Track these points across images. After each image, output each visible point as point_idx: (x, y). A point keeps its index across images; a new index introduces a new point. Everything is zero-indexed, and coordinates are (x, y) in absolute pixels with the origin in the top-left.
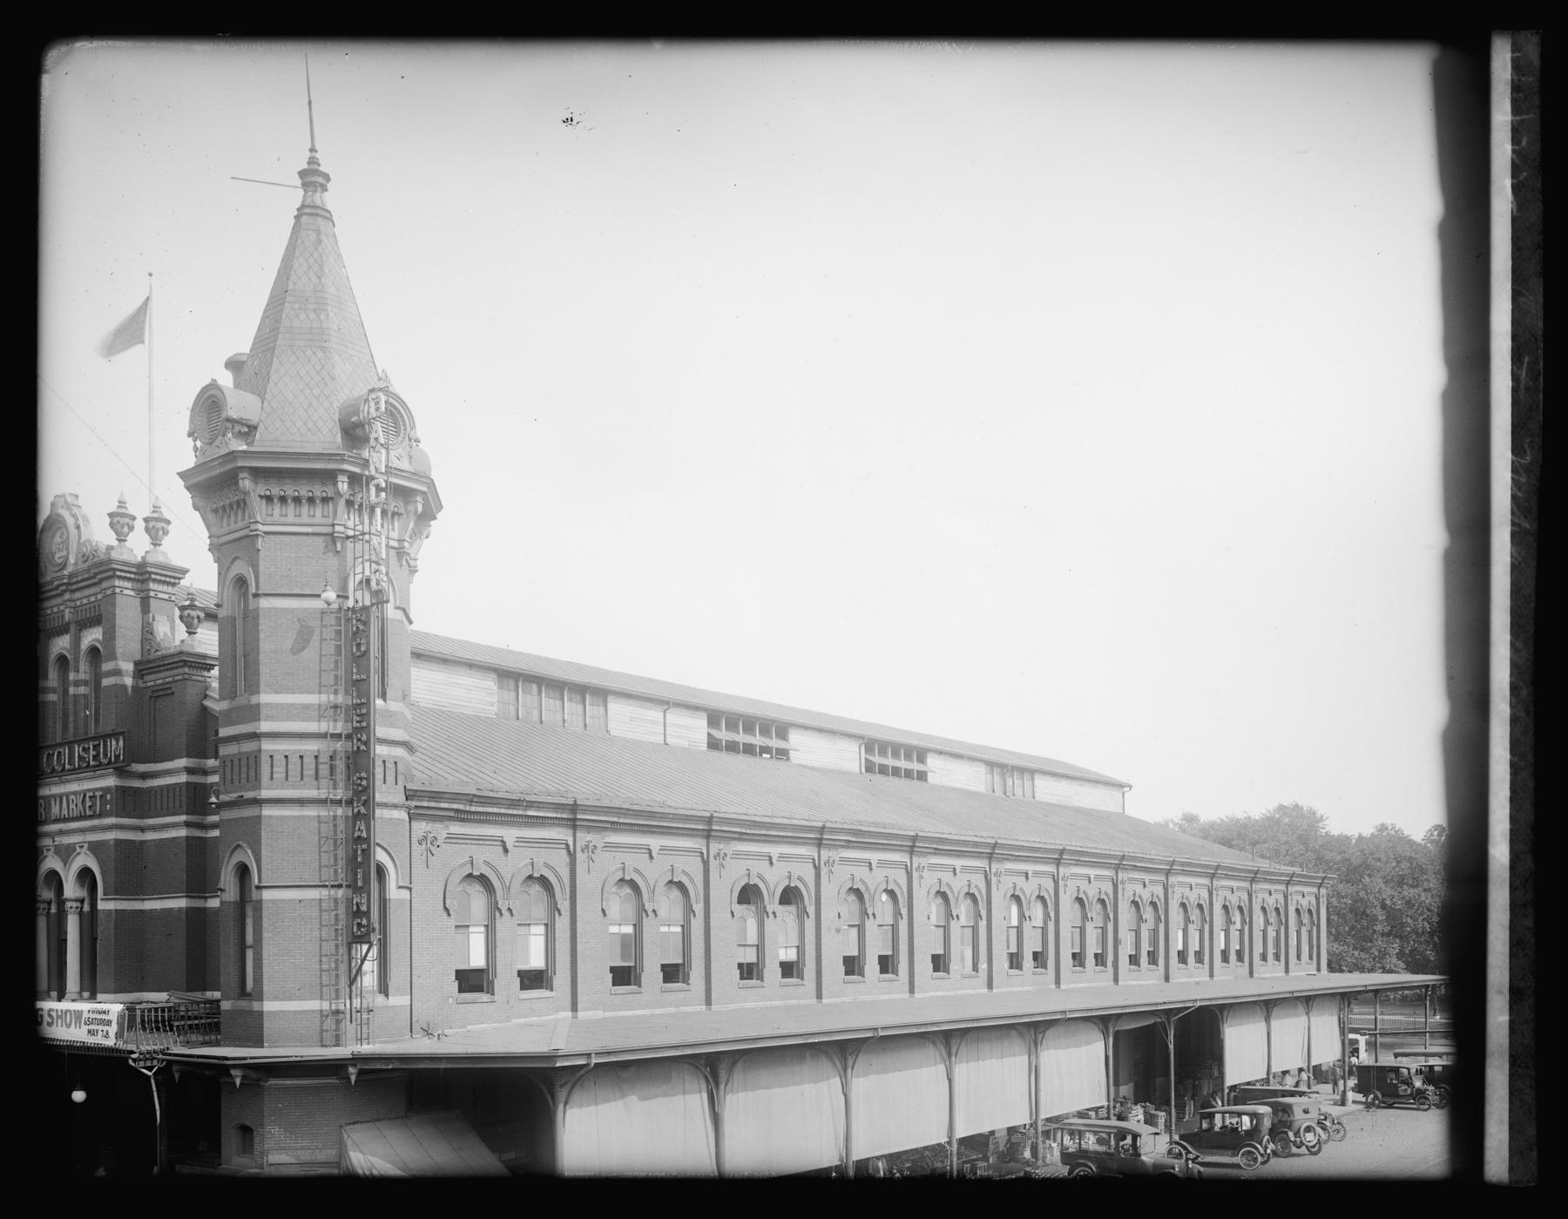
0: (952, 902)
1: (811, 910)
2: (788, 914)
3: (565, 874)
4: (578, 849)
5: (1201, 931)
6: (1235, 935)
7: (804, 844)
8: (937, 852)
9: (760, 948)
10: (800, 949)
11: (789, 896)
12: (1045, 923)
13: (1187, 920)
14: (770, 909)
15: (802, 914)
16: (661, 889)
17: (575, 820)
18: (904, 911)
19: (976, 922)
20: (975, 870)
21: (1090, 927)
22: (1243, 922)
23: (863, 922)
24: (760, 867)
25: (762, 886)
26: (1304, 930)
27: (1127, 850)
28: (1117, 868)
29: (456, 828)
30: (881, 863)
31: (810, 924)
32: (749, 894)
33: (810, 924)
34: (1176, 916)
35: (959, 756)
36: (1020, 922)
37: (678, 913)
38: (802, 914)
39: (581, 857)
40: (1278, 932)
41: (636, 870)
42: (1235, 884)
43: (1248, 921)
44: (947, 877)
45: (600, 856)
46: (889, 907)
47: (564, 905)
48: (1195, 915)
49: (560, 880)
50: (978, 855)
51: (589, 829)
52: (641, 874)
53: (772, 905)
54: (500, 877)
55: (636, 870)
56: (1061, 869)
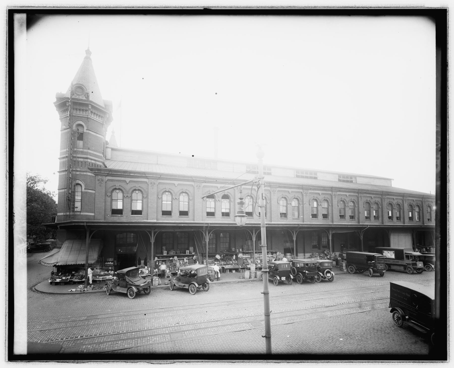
25: (229, 194)
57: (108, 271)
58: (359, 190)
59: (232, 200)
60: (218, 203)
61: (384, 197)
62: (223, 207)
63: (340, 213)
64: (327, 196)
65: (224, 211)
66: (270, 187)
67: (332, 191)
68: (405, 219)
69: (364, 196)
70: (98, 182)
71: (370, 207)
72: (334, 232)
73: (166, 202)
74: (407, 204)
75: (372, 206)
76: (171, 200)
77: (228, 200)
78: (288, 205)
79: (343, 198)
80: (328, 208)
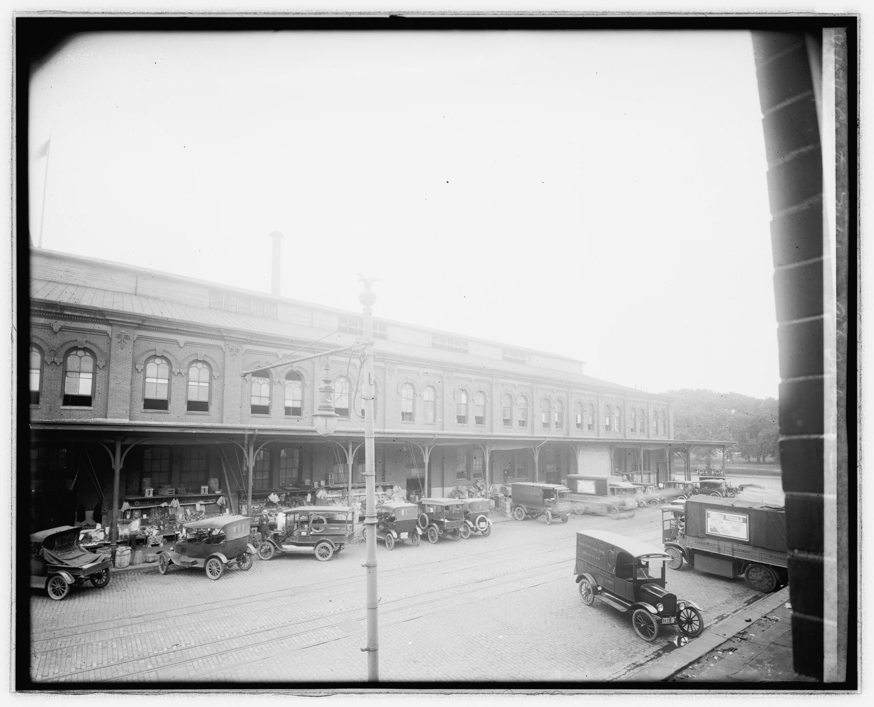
25: (303, 373)
59: (308, 383)
76: (167, 376)
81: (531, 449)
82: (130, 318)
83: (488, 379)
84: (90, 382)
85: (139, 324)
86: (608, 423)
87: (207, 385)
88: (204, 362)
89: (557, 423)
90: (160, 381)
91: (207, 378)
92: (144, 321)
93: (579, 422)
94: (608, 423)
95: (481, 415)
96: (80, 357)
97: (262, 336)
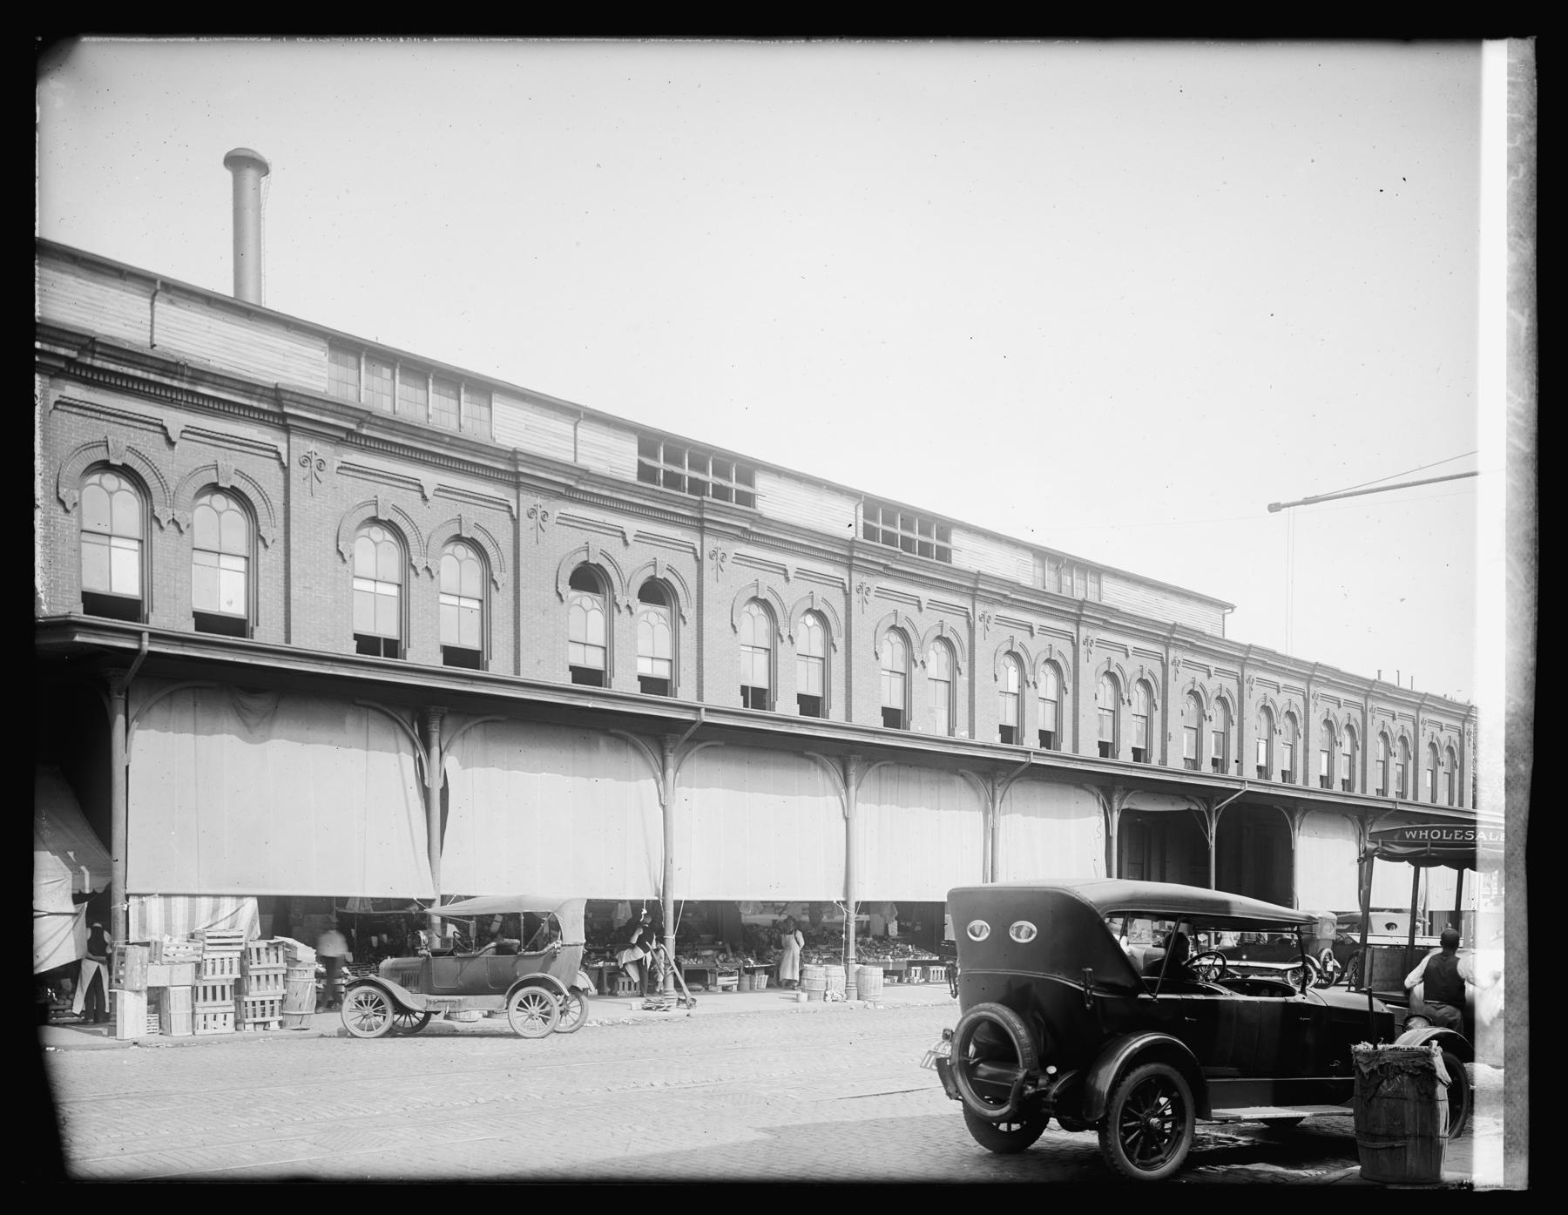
0: (915, 644)
1: (690, 613)
2: (653, 618)
3: (506, 541)
4: (706, 553)
5: (1451, 776)
6: (1443, 781)
7: (261, 422)
8: (1106, 626)
9: (608, 650)
10: (674, 663)
11: (655, 592)
12: (1060, 696)
13: (1437, 762)
14: (622, 601)
15: (678, 618)
16: (1213, 701)
17: (851, 558)
18: (840, 642)
19: (1295, 740)
20: (953, 609)
21: (1393, 761)
22: (1354, 746)
23: (775, 644)
24: (613, 545)
25: (610, 569)
26: (1441, 770)
27: (1179, 621)
28: (1419, 708)
29: (74, 391)
30: (1137, 651)
31: (688, 633)
32: (588, 578)
33: (688, 633)
34: (1425, 754)
35: (238, 255)
36: (1387, 758)
37: (474, 585)
38: (678, 618)
39: (708, 563)
40: (1405, 767)
41: (670, 569)
42: (1445, 721)
43: (1411, 755)
44: (1201, 677)
45: (329, 475)
46: (818, 633)
47: (504, 578)
48: (1444, 757)
49: (959, 640)
50: (1153, 638)
51: (987, 601)
52: (485, 531)
53: (627, 595)
54: (782, 604)
55: (670, 569)
56: (1083, 629)
57: (1223, 968)
58: (1174, 627)
59: (690, 613)
60: (621, 620)
61: (1248, 672)
62: (644, 646)
63: (1101, 732)
64: (820, 591)
65: (646, 668)
66: (850, 567)
67: (1078, 623)
68: (843, 689)
69: (1001, 620)
70: (532, 522)
71: (1202, 716)
72: (1125, 806)
73: (368, 586)
74: (1318, 714)
75: (1208, 713)
76: (396, 578)
77: (663, 610)
78: (916, 671)
79: (1115, 661)
80: (1058, 705)
81: (1200, 813)
82: (310, 407)
83: (1236, 669)
84: (241, 579)
85: (349, 432)
86: (1324, 773)
87: (394, 591)
88: (126, 472)
89: (1284, 772)
90: (464, 602)
91: (394, 573)
92: (976, 581)
93: (1262, 762)
94: (1324, 773)
95: (816, 691)
96: (111, 493)
97: (200, 375)
